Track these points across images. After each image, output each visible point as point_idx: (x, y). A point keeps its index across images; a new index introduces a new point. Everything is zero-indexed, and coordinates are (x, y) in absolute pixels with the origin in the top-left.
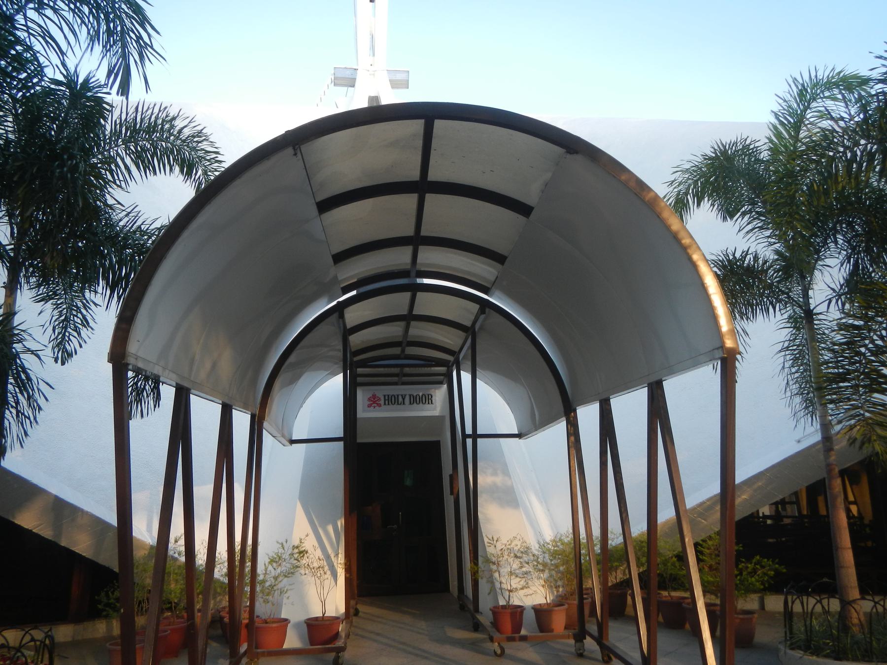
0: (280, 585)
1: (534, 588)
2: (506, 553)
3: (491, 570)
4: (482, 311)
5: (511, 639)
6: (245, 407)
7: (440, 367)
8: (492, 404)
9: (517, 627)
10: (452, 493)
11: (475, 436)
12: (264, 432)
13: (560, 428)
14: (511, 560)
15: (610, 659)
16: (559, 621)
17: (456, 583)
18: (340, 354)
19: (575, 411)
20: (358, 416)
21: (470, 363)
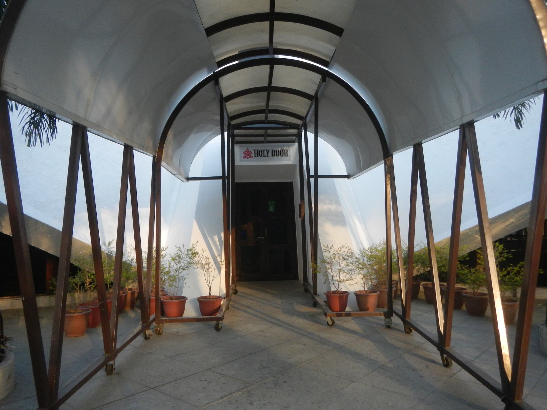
0: (180, 275)
1: (356, 280)
2: (337, 256)
3: (326, 268)
4: (323, 80)
5: (340, 315)
6: (144, 149)
7: (290, 130)
8: (330, 155)
9: (343, 306)
10: (300, 217)
11: (317, 176)
12: (162, 168)
13: (380, 169)
14: (340, 261)
15: (411, 331)
16: (372, 300)
17: (302, 274)
19: (392, 155)
21: (313, 126)
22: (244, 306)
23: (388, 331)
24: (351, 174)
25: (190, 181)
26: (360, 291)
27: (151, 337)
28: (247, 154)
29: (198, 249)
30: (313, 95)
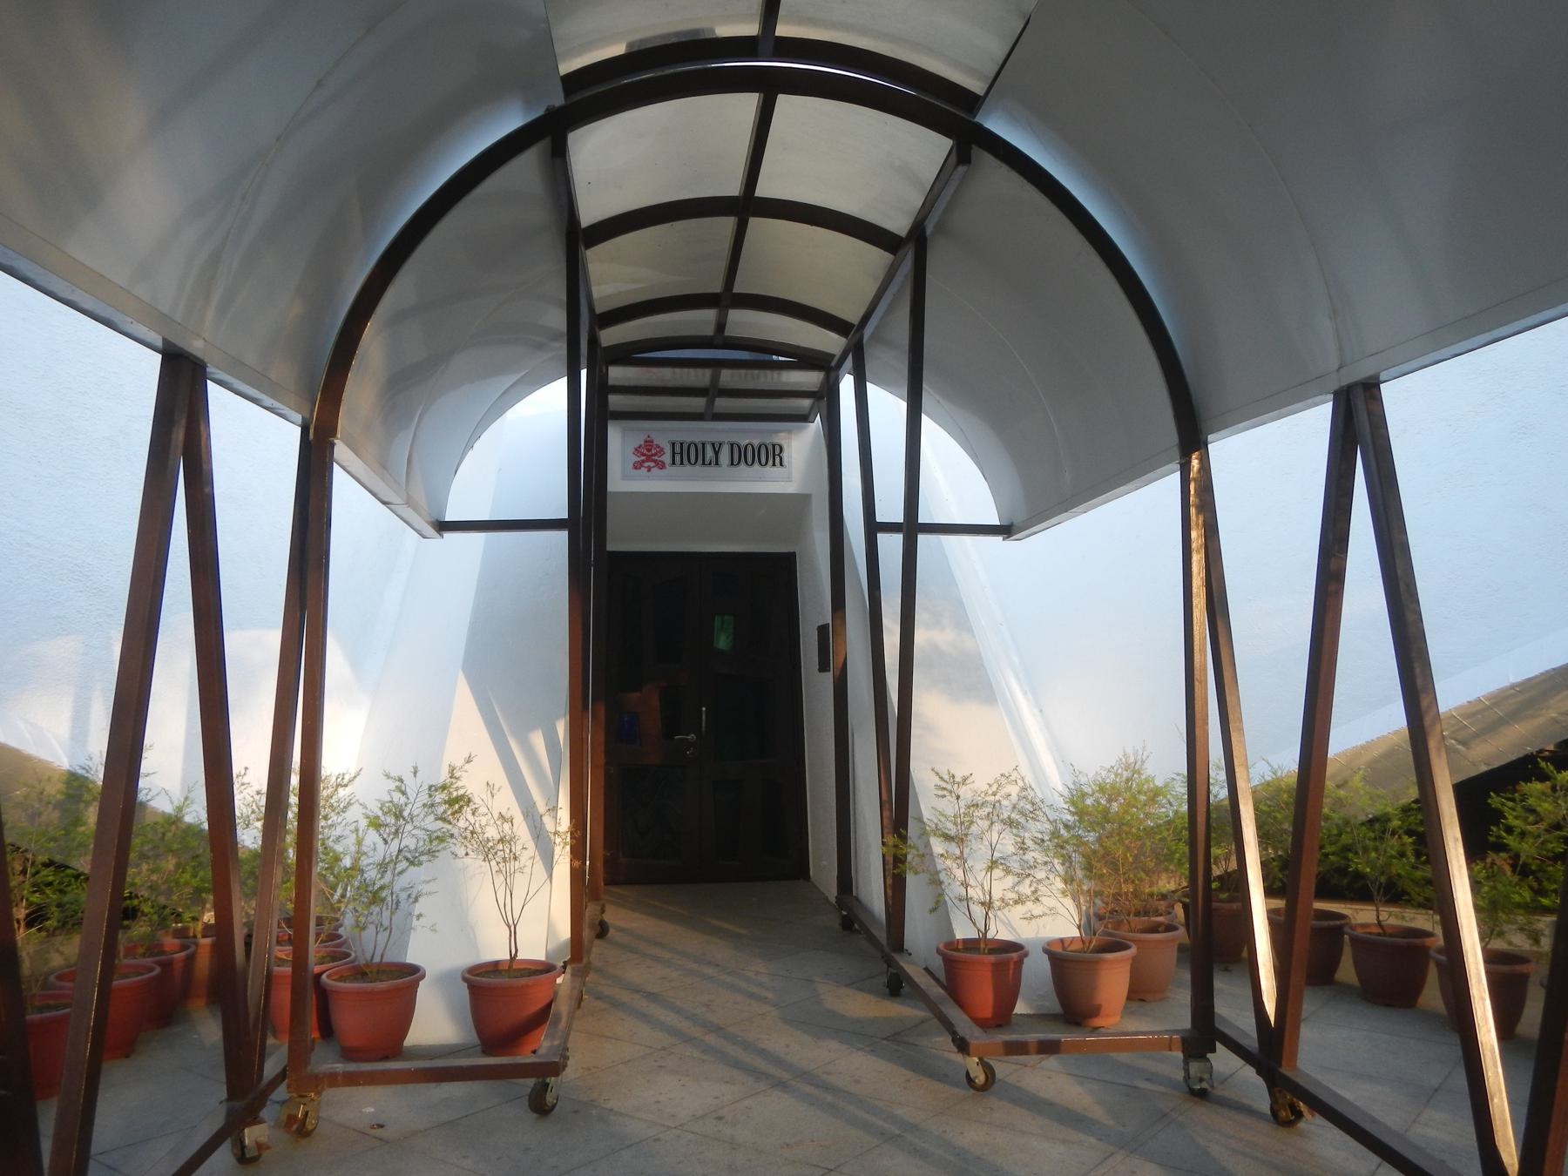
6: (258, 386)
10: (824, 667)
11: (911, 528)
12: (338, 475)
13: (1162, 494)
18: (557, 319)
20: (610, 489)
22: (637, 990)
23: (1201, 1112)
24: (1017, 520)
25: (448, 536)
26: (1062, 940)
27: (266, 1154)
28: (647, 456)
29: (471, 784)
30: (903, 233)
